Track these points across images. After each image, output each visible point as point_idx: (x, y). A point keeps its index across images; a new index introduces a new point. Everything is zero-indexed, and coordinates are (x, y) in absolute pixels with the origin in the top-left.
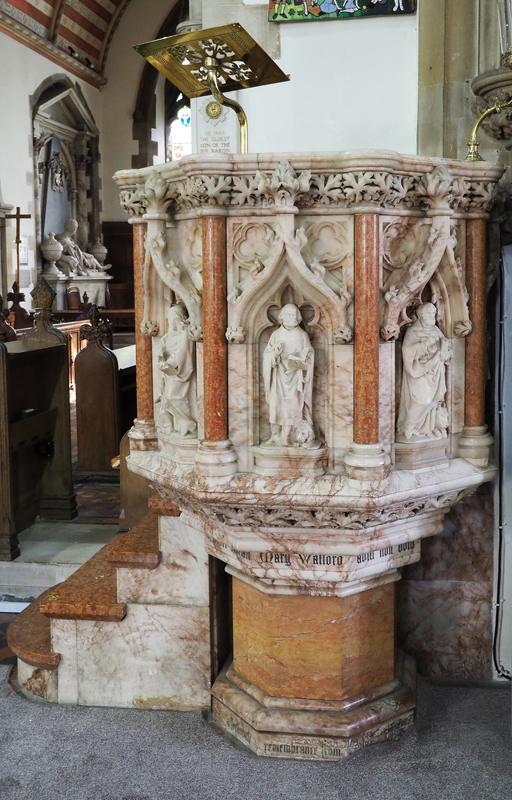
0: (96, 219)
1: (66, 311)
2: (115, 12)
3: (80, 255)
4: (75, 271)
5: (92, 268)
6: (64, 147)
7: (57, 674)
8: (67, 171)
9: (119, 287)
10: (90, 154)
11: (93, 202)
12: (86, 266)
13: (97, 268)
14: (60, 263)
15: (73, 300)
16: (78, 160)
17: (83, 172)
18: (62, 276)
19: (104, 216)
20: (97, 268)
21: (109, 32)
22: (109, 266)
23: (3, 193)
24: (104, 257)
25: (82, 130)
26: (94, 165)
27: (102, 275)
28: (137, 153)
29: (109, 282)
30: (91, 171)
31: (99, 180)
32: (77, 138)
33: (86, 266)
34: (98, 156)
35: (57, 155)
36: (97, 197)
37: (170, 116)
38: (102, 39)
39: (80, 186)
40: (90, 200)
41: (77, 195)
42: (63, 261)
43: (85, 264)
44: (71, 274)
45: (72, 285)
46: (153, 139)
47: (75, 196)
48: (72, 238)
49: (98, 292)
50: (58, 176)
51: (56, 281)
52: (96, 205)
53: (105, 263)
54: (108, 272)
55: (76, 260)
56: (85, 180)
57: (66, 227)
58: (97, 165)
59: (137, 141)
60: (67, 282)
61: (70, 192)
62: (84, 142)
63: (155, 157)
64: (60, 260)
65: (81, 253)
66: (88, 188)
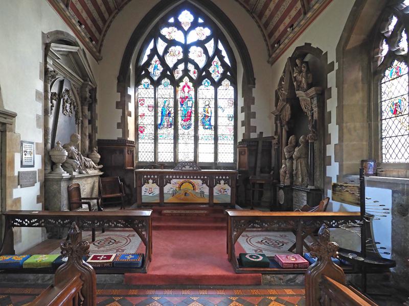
0: (94, 137)
1: (46, 213)
2: (108, 19)
3: (81, 159)
4: (77, 170)
5: (90, 167)
6: (73, 88)
7: (45, 176)
8: (75, 104)
9: (107, 179)
10: (90, 97)
11: (92, 127)
12: (86, 167)
13: (94, 167)
14: (66, 165)
15: (74, 193)
16: (83, 100)
17: (86, 108)
18: (66, 175)
19: (98, 136)
20: (94, 167)
21: (104, 30)
22: (101, 166)
23: (4, 97)
24: (98, 160)
25: (87, 81)
26: (93, 105)
27: (96, 172)
28: (119, 100)
29: (101, 176)
30: (91, 109)
31: (96, 115)
32: (83, 87)
33: (86, 167)
34: (95, 101)
35: (67, 91)
36: (95, 124)
37: (138, 83)
38: (100, 33)
39: (84, 116)
40: (90, 126)
41: (82, 121)
42: (67, 163)
43: (85, 165)
44: (74, 173)
45: (75, 182)
46: (129, 93)
47: (80, 121)
48: (77, 147)
49: (94, 183)
50: (68, 105)
51: (61, 179)
52: (94, 129)
53: (99, 164)
54: (101, 170)
55: (78, 162)
56: (87, 113)
57: (73, 139)
58: (95, 106)
59: (120, 93)
60: (70, 179)
61: (77, 118)
62: (87, 90)
63: (129, 103)
64: (66, 162)
65: (83, 158)
66: (90, 118)
